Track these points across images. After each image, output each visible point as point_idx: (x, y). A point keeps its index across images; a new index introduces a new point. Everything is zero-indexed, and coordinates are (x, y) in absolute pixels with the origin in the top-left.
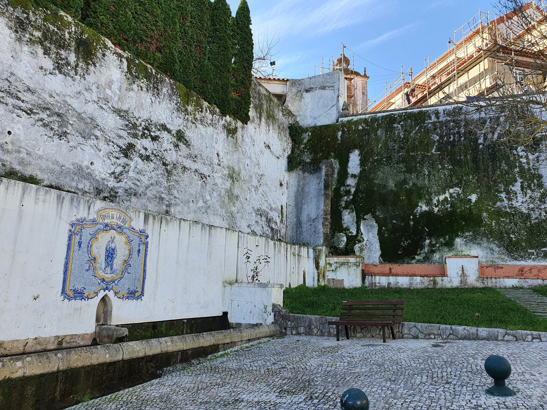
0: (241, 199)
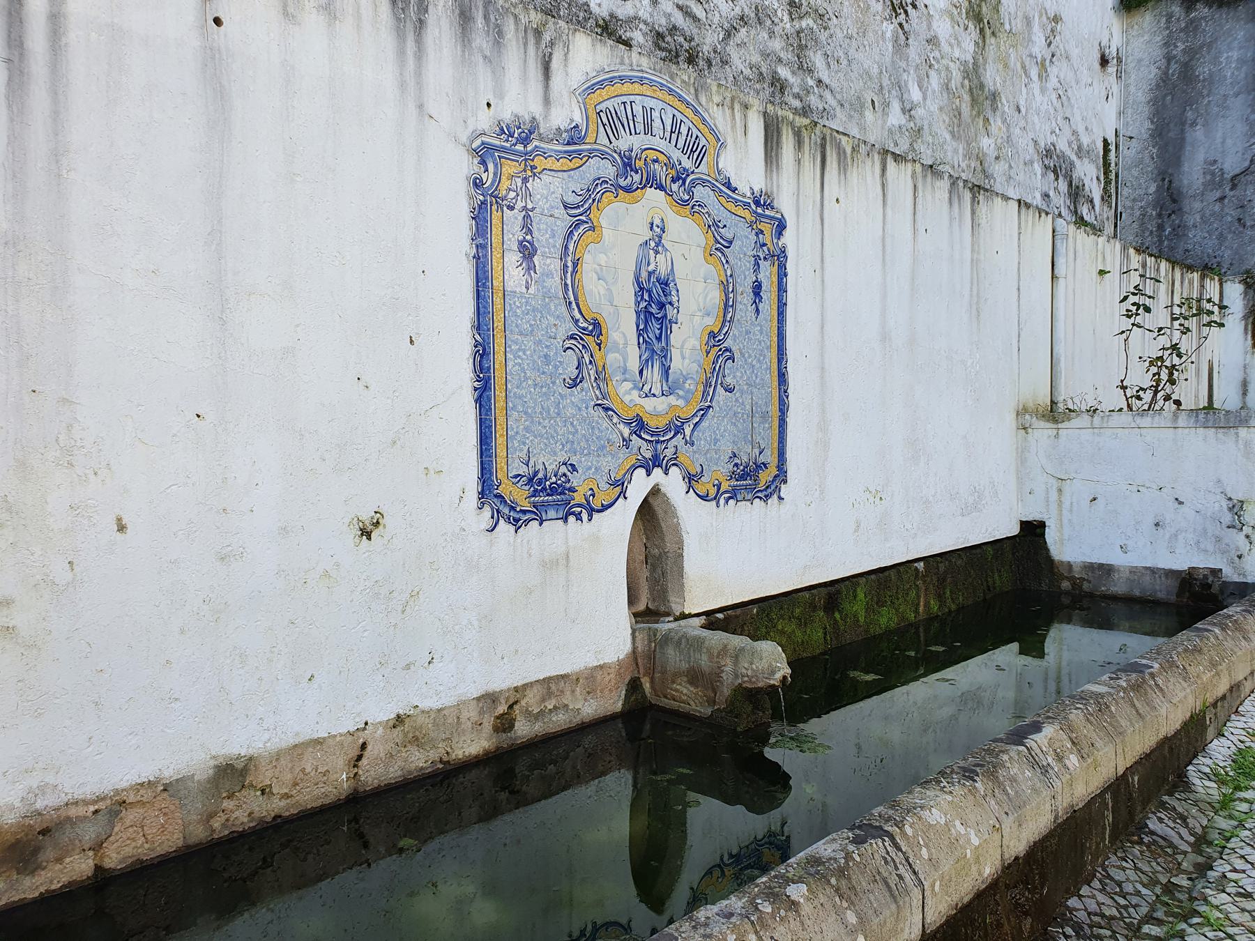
0: (1005, 106)
